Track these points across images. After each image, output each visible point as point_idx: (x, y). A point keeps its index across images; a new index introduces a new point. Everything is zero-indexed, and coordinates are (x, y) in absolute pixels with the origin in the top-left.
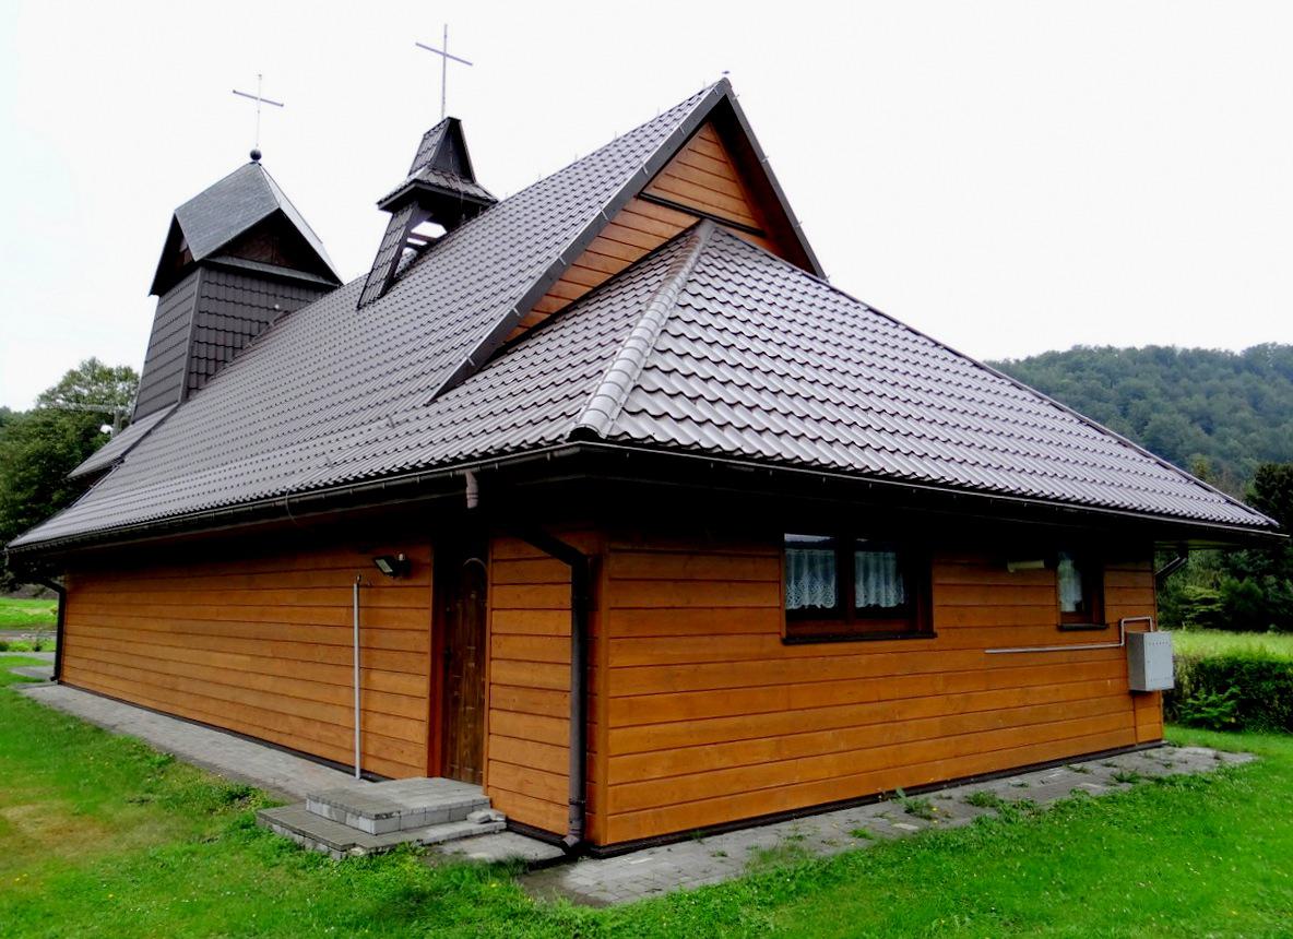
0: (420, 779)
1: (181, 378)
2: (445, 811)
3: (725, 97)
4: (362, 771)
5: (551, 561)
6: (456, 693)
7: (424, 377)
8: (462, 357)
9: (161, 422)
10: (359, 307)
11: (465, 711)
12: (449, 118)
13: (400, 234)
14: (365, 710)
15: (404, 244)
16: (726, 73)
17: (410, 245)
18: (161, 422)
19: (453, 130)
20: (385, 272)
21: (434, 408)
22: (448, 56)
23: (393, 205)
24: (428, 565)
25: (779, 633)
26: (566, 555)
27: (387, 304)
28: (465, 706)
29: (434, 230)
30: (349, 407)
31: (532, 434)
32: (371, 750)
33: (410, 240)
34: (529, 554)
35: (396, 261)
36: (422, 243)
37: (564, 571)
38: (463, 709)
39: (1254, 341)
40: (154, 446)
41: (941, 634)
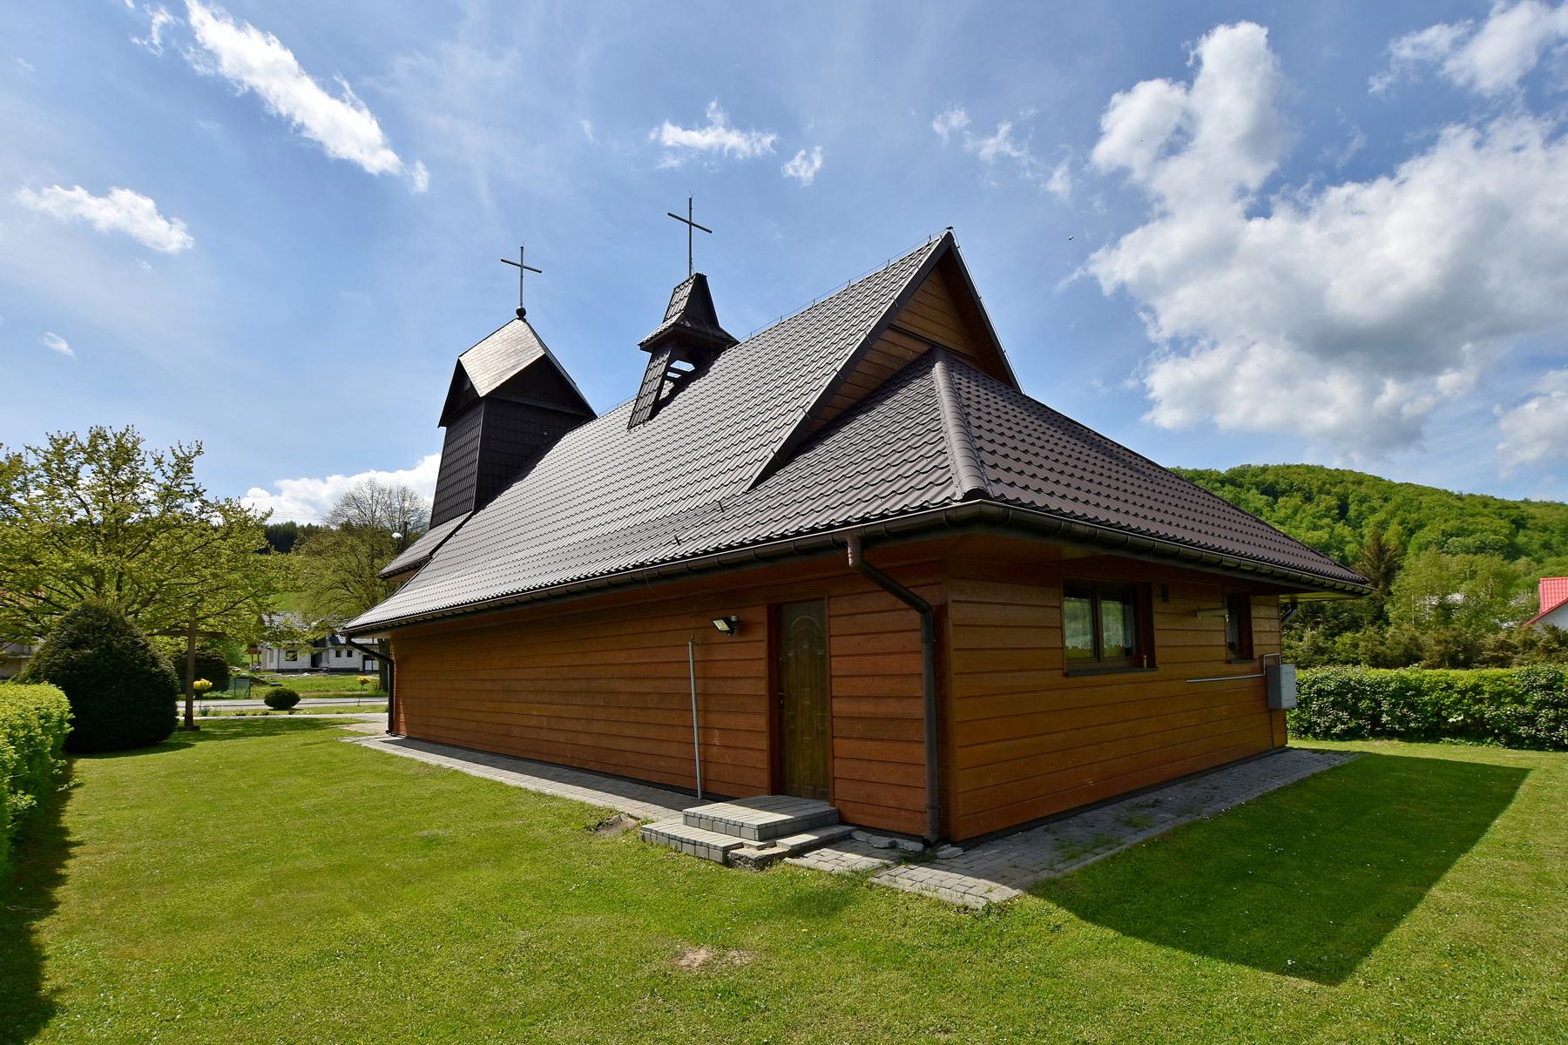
0: (764, 796)
1: (473, 492)
2: (806, 820)
3: (950, 247)
4: (703, 792)
5: (911, 611)
6: (792, 727)
7: (596, 508)
8: (769, 454)
9: (460, 526)
10: (630, 427)
11: (802, 740)
12: (697, 274)
13: (662, 369)
14: (706, 744)
15: (665, 377)
16: (950, 228)
17: (671, 379)
18: (460, 526)
19: (700, 283)
20: (652, 398)
21: (755, 494)
22: (687, 222)
23: (654, 346)
24: (762, 623)
25: (1063, 669)
26: (915, 603)
27: (655, 425)
28: (802, 737)
29: (688, 367)
30: (568, 522)
31: (737, 536)
32: (712, 775)
33: (669, 374)
34: (364, 682)
35: (660, 389)
36: (677, 376)
37: (914, 617)
38: (800, 739)
39: (1236, 464)
40: (454, 547)
41: (1161, 667)
